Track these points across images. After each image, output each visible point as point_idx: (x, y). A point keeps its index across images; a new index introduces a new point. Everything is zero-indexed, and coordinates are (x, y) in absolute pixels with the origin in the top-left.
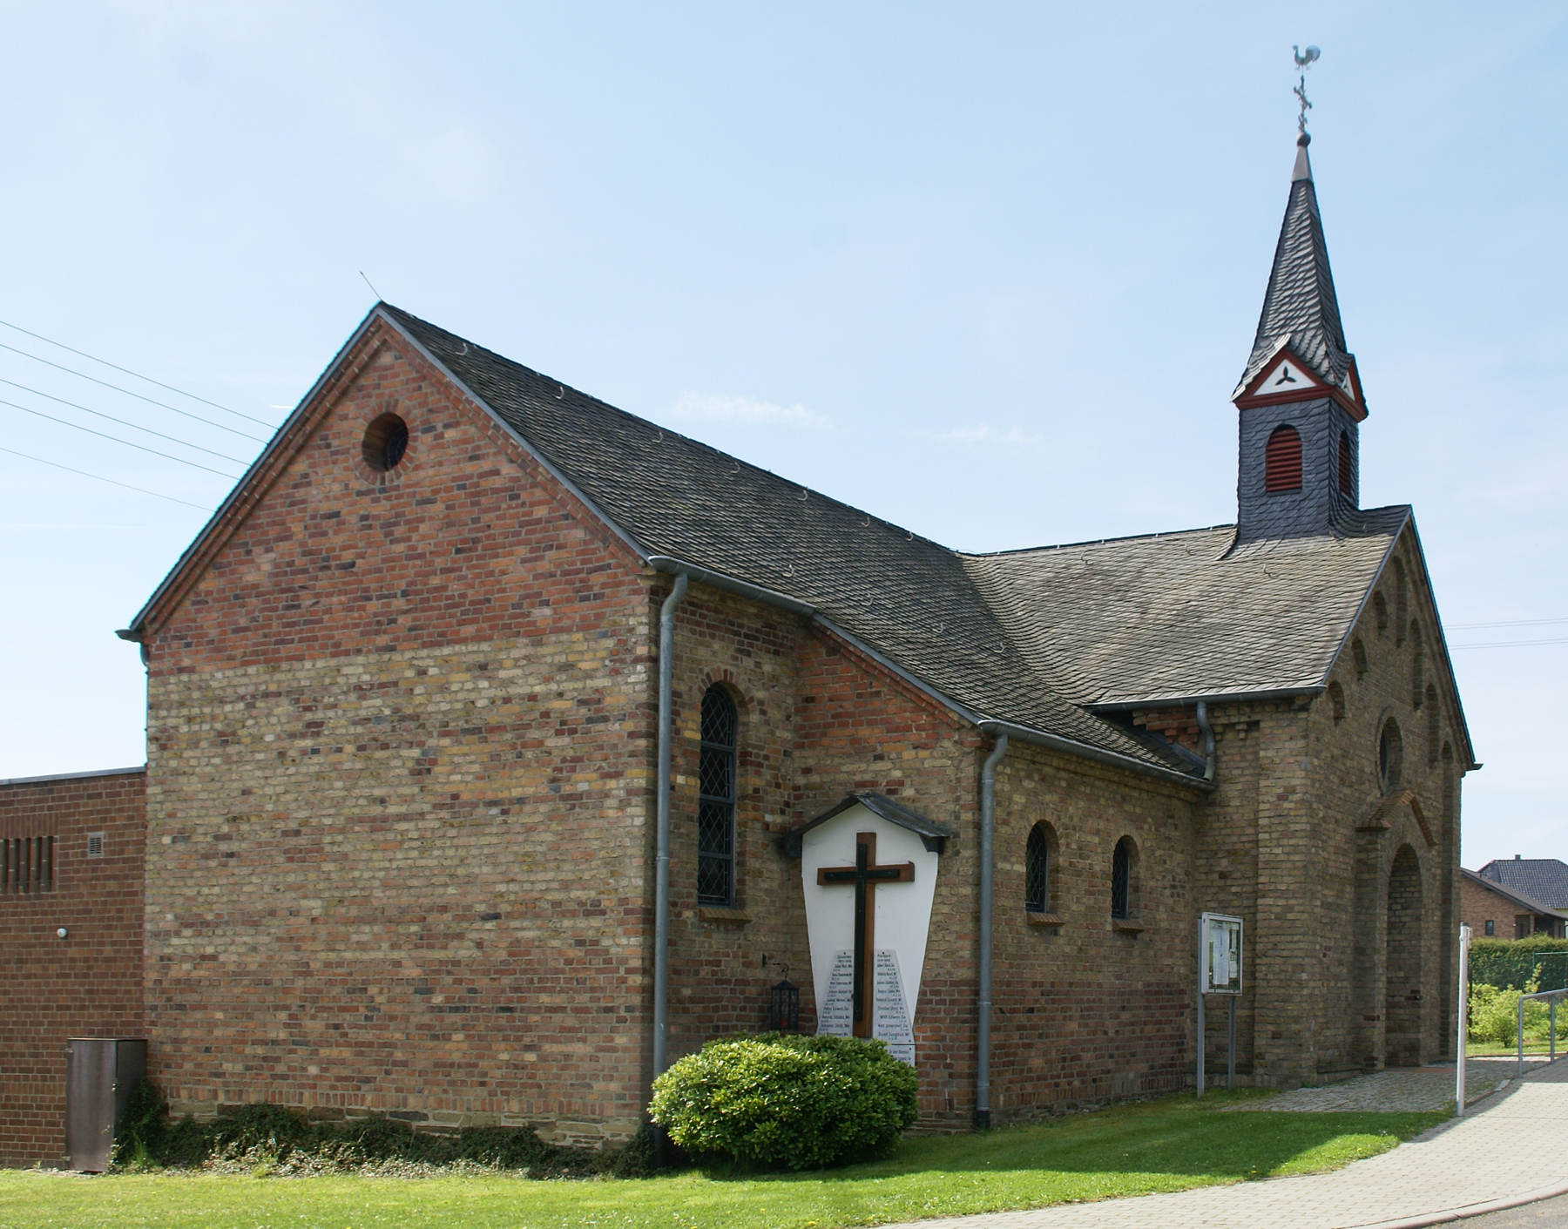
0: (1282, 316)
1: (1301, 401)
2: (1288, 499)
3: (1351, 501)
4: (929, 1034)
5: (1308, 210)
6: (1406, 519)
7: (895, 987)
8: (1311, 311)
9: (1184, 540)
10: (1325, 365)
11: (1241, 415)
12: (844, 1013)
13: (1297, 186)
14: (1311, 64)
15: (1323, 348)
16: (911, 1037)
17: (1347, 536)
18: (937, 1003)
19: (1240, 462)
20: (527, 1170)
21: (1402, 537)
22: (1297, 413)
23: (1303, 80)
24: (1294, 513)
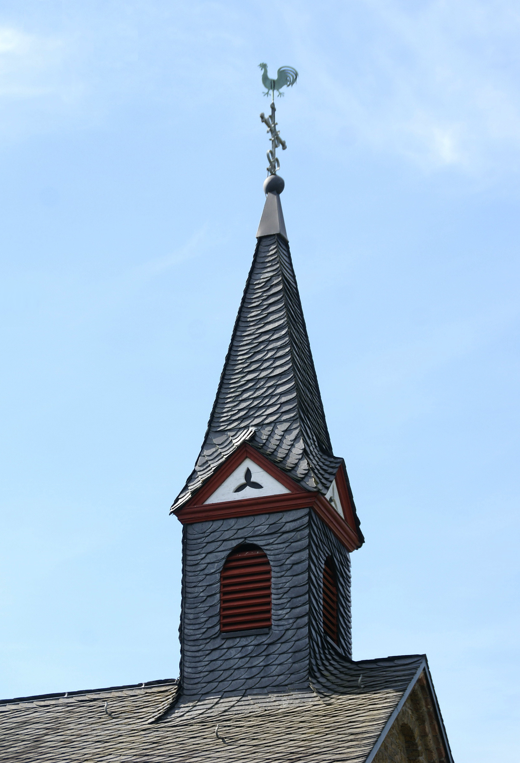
0: (243, 405)
1: (270, 512)
2: (252, 641)
3: (340, 651)
5: (279, 272)
6: (419, 674)
8: (284, 399)
9: (104, 700)
10: (304, 465)
11: (185, 532)
13: (265, 242)
14: (284, 89)
15: (300, 445)
17: (336, 692)
19: (184, 592)
21: (413, 696)
22: (263, 529)
23: (273, 109)
24: (259, 661)
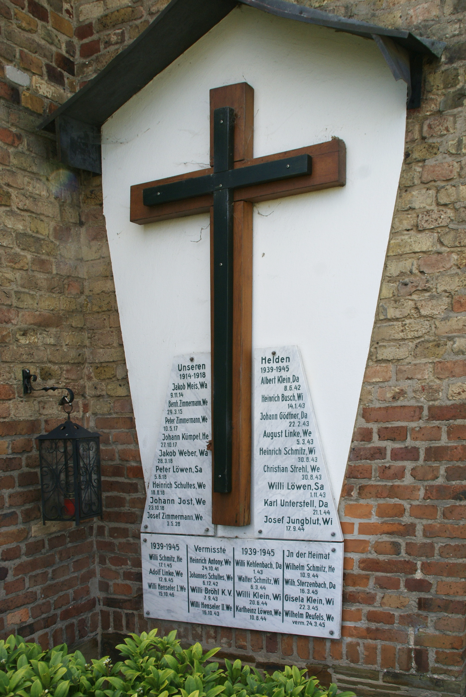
4: (374, 519)
7: (433, 443)
12: (195, 478)
16: (336, 527)
18: (396, 455)
20: (120, 654)
